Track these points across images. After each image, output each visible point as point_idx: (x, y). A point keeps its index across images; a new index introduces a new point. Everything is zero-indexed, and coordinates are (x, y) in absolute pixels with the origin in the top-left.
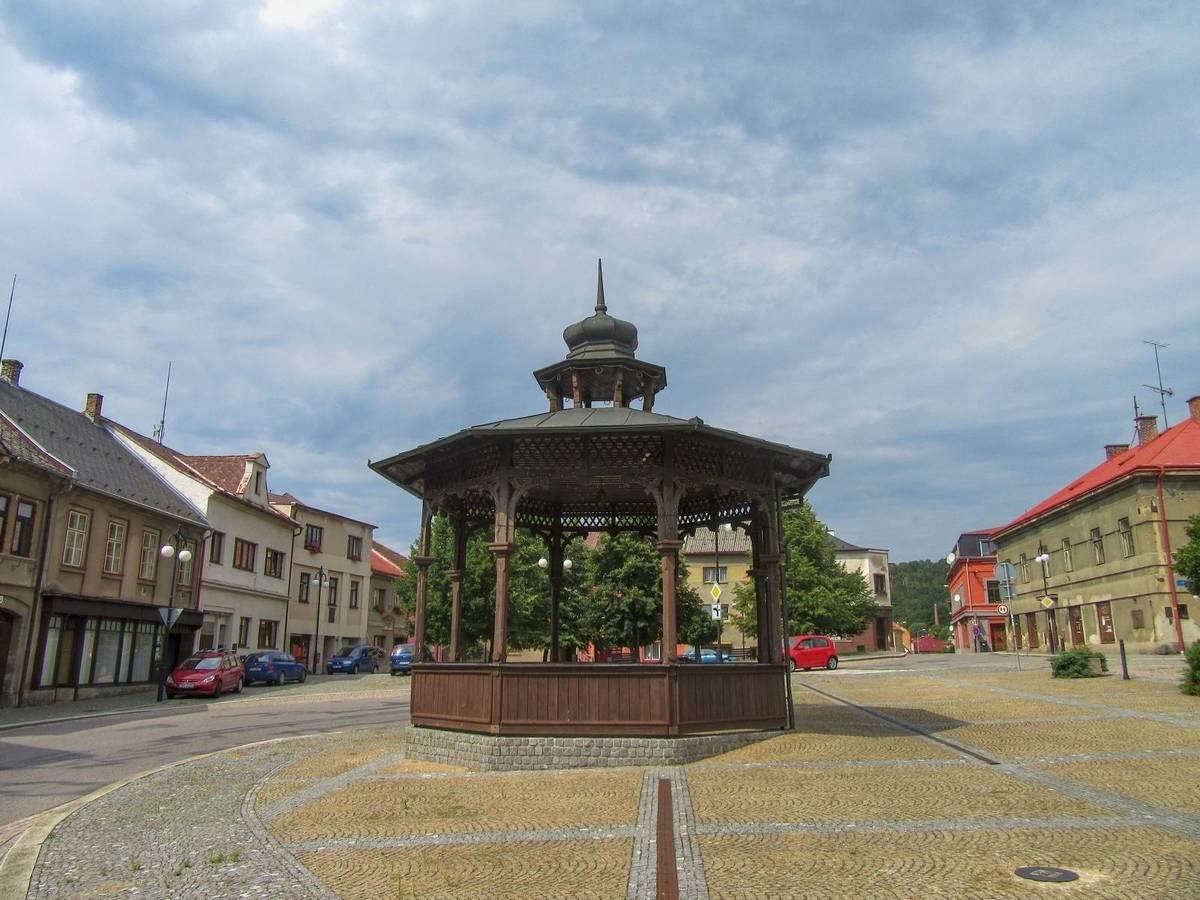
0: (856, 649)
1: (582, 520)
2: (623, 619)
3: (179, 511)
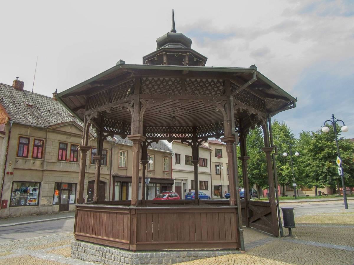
0: (57, 208)
1: (156, 135)
2: (326, 176)
3: (160, 148)
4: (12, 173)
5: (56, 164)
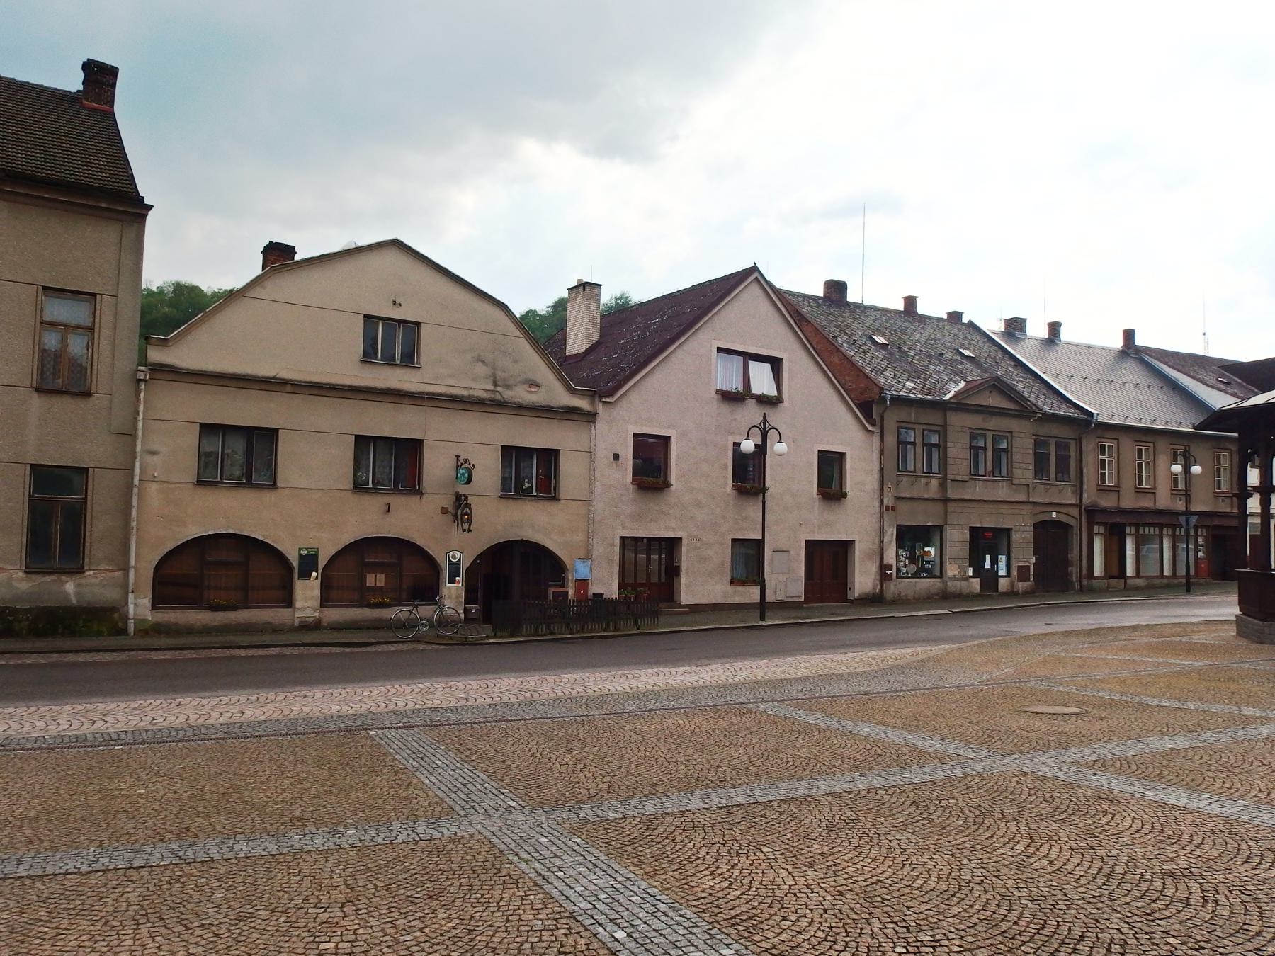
4: (893, 508)
5: (967, 484)
